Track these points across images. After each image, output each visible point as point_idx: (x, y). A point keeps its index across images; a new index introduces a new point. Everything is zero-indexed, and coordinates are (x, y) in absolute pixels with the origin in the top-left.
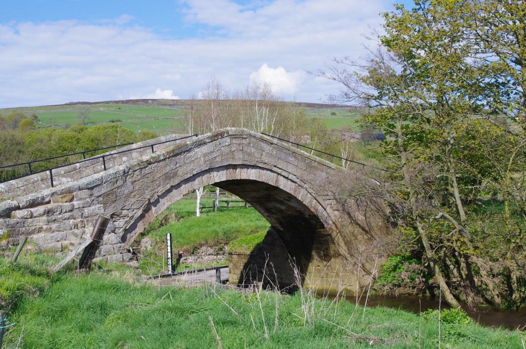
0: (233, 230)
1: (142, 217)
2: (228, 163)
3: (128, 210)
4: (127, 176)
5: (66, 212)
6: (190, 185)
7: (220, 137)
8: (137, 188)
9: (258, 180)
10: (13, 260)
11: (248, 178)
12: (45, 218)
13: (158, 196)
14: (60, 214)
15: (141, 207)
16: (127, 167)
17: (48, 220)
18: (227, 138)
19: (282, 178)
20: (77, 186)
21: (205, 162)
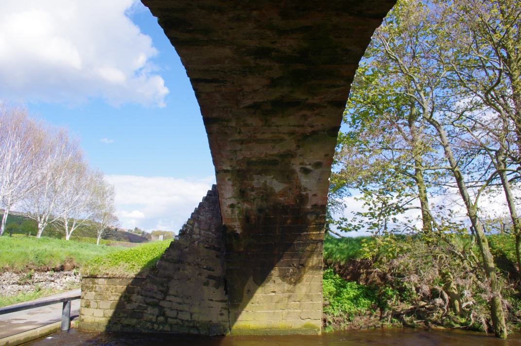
0: (46, 254)
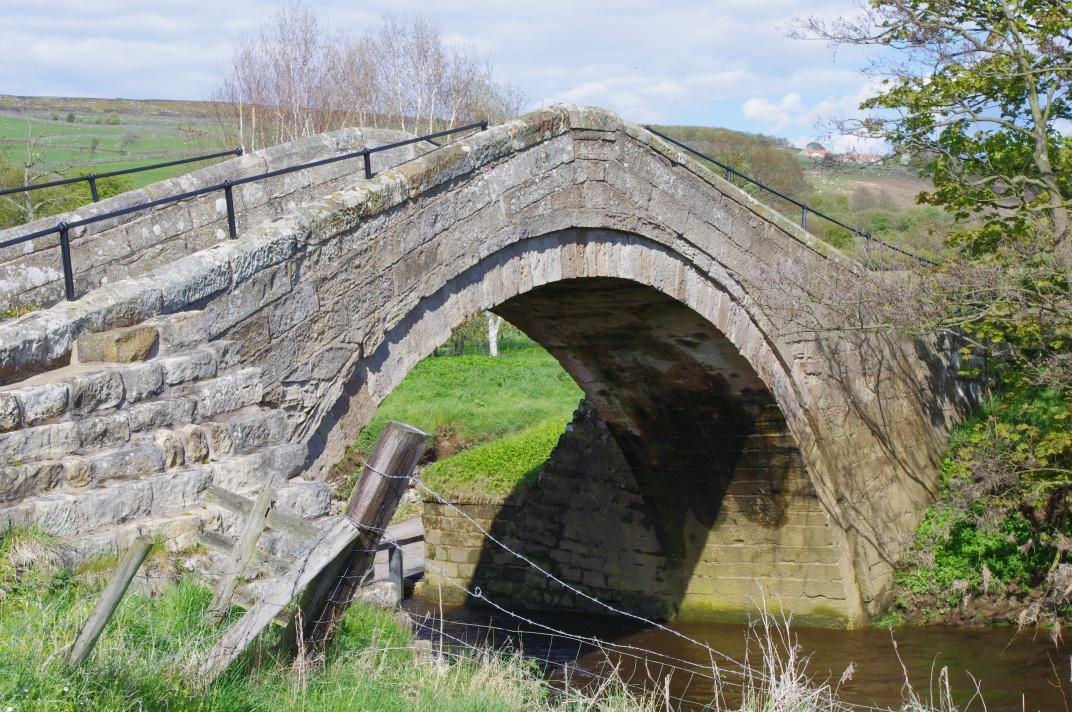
1: (340, 408)
2: (562, 224)
3: (303, 383)
4: (303, 258)
5: (139, 400)
6: (469, 294)
7: (548, 134)
8: (329, 304)
9: (638, 279)
10: (75, 656)
11: (614, 275)
12: (67, 425)
13: (386, 332)
14: (118, 407)
15: (339, 371)
16: (303, 228)
17: (79, 433)
18: (565, 138)
19: (692, 274)
20: (155, 295)
21: (510, 215)
